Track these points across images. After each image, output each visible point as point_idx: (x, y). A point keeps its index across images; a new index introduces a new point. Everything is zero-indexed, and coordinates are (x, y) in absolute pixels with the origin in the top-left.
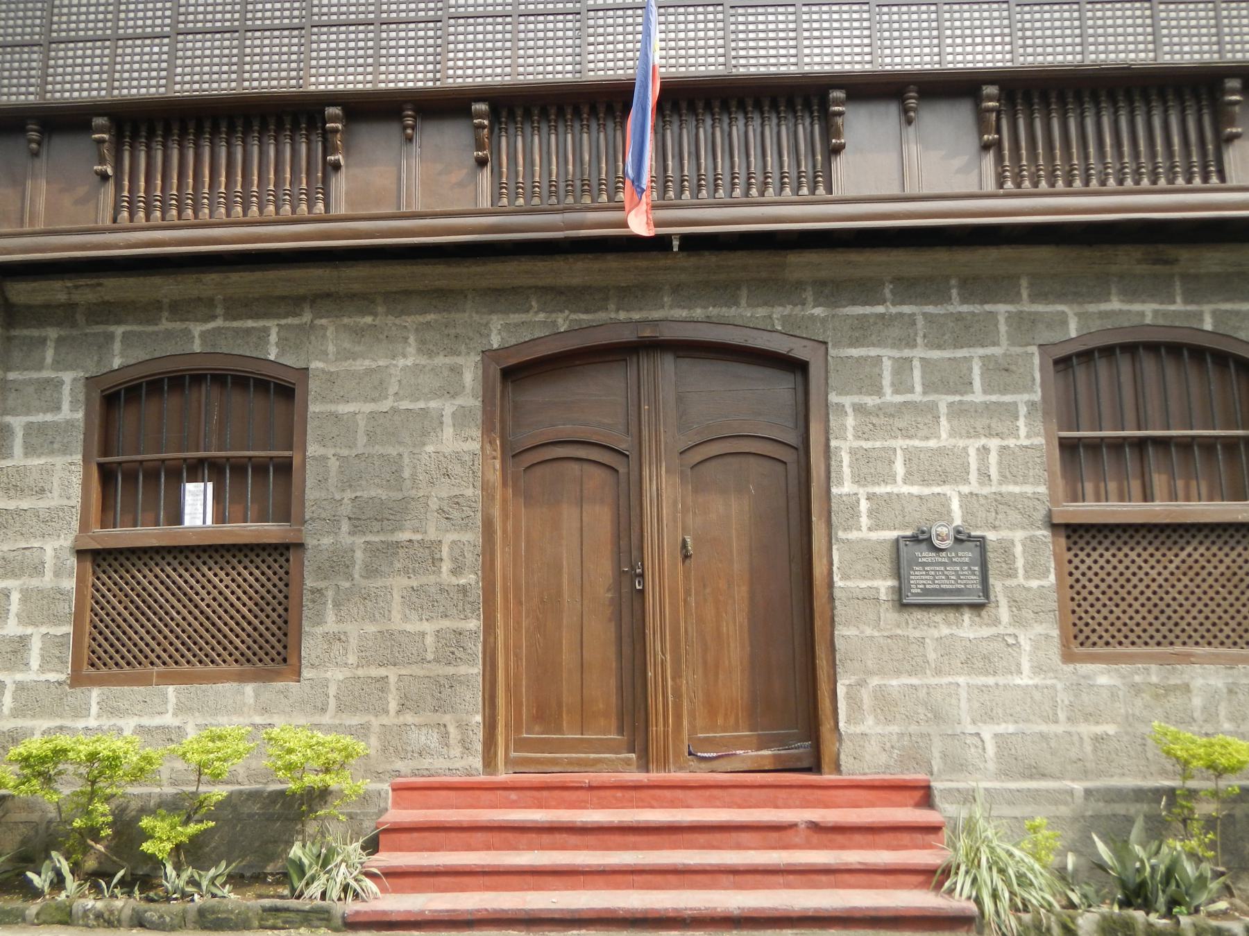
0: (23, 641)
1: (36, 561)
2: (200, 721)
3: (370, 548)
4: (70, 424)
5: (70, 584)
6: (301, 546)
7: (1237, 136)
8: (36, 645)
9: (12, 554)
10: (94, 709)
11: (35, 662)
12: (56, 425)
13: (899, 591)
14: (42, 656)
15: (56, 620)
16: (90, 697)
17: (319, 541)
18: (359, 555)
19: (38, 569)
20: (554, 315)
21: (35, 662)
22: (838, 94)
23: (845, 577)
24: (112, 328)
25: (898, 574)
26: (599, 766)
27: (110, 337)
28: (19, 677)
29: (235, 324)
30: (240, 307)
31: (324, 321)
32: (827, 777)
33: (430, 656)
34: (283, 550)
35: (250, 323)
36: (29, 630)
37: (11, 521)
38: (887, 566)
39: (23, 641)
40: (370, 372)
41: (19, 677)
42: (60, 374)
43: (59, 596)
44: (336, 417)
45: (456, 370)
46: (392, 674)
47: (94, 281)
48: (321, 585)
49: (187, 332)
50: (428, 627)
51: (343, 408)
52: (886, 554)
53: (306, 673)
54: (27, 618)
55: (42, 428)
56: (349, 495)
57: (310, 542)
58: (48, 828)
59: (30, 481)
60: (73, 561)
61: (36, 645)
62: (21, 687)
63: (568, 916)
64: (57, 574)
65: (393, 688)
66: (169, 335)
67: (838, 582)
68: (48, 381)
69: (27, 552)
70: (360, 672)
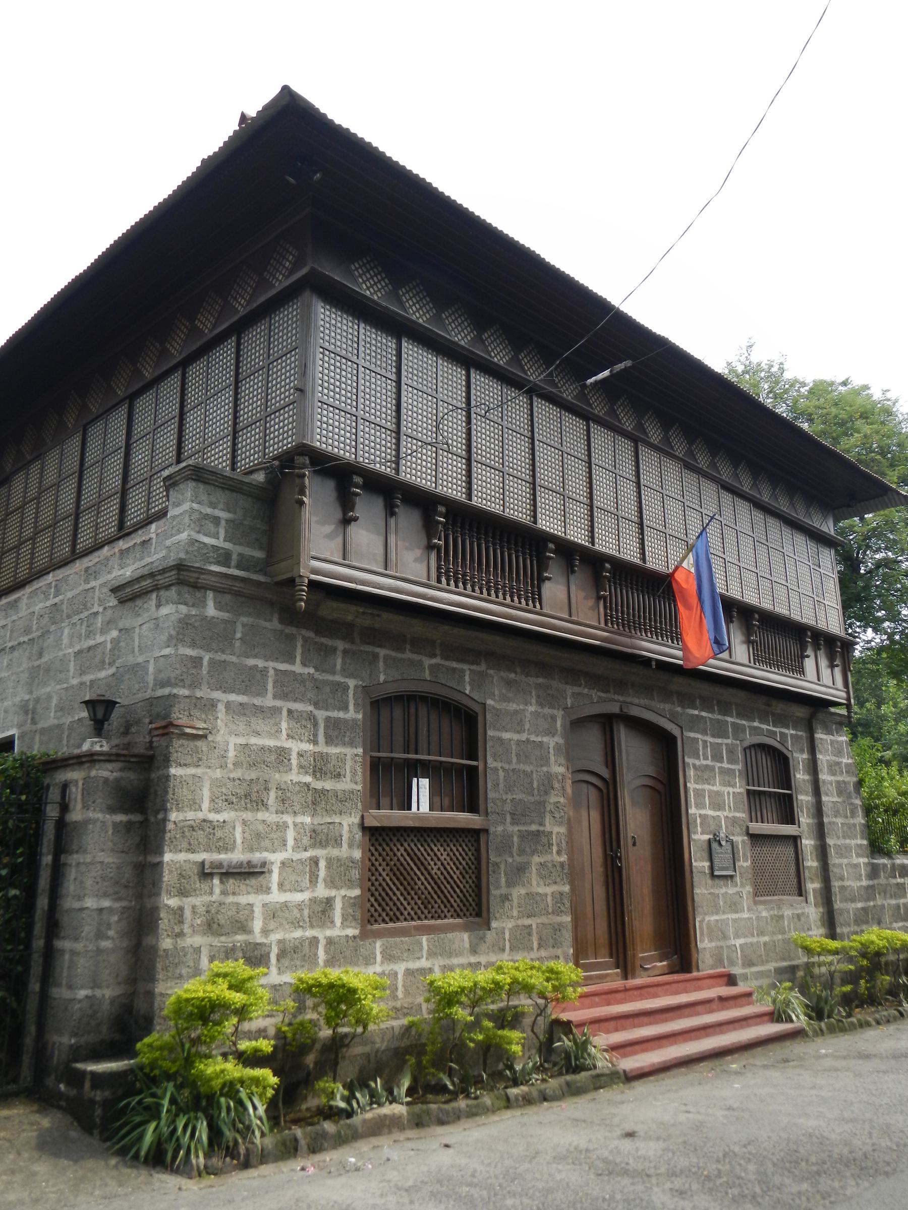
0: (329, 901)
1: (337, 834)
2: (442, 963)
3: (523, 836)
4: (354, 721)
5: (357, 854)
6: (486, 831)
7: (549, 579)
8: (338, 905)
9: (320, 827)
10: (379, 958)
11: (338, 920)
12: (346, 721)
13: (712, 868)
14: (343, 915)
15: (350, 885)
16: (375, 948)
17: (502, 829)
18: (515, 839)
19: (338, 842)
20: (592, 691)
21: (338, 920)
22: (358, 480)
23: (695, 861)
24: (377, 650)
25: (711, 859)
26: (608, 979)
27: (334, 650)
28: (329, 933)
29: (447, 663)
30: (454, 652)
31: (491, 672)
32: (695, 974)
33: (550, 910)
34: (475, 835)
35: (455, 665)
36: (333, 893)
37: (318, 799)
38: (705, 855)
39: (329, 901)
40: (516, 712)
41: (329, 933)
42: (347, 680)
43: (351, 864)
44: (500, 739)
45: (553, 718)
46: (532, 922)
47: (375, 612)
48: (498, 860)
49: (420, 663)
50: (548, 890)
51: (506, 736)
52: (705, 846)
53: (494, 924)
54: (331, 883)
55: (337, 721)
56: (510, 797)
57: (492, 830)
58: (376, 1056)
59: (330, 766)
60: (359, 835)
61: (338, 905)
62: (330, 941)
63: (662, 1066)
64: (350, 846)
65: (534, 932)
66: (412, 663)
67: (694, 864)
68: (339, 684)
69: (331, 827)
70: (520, 922)
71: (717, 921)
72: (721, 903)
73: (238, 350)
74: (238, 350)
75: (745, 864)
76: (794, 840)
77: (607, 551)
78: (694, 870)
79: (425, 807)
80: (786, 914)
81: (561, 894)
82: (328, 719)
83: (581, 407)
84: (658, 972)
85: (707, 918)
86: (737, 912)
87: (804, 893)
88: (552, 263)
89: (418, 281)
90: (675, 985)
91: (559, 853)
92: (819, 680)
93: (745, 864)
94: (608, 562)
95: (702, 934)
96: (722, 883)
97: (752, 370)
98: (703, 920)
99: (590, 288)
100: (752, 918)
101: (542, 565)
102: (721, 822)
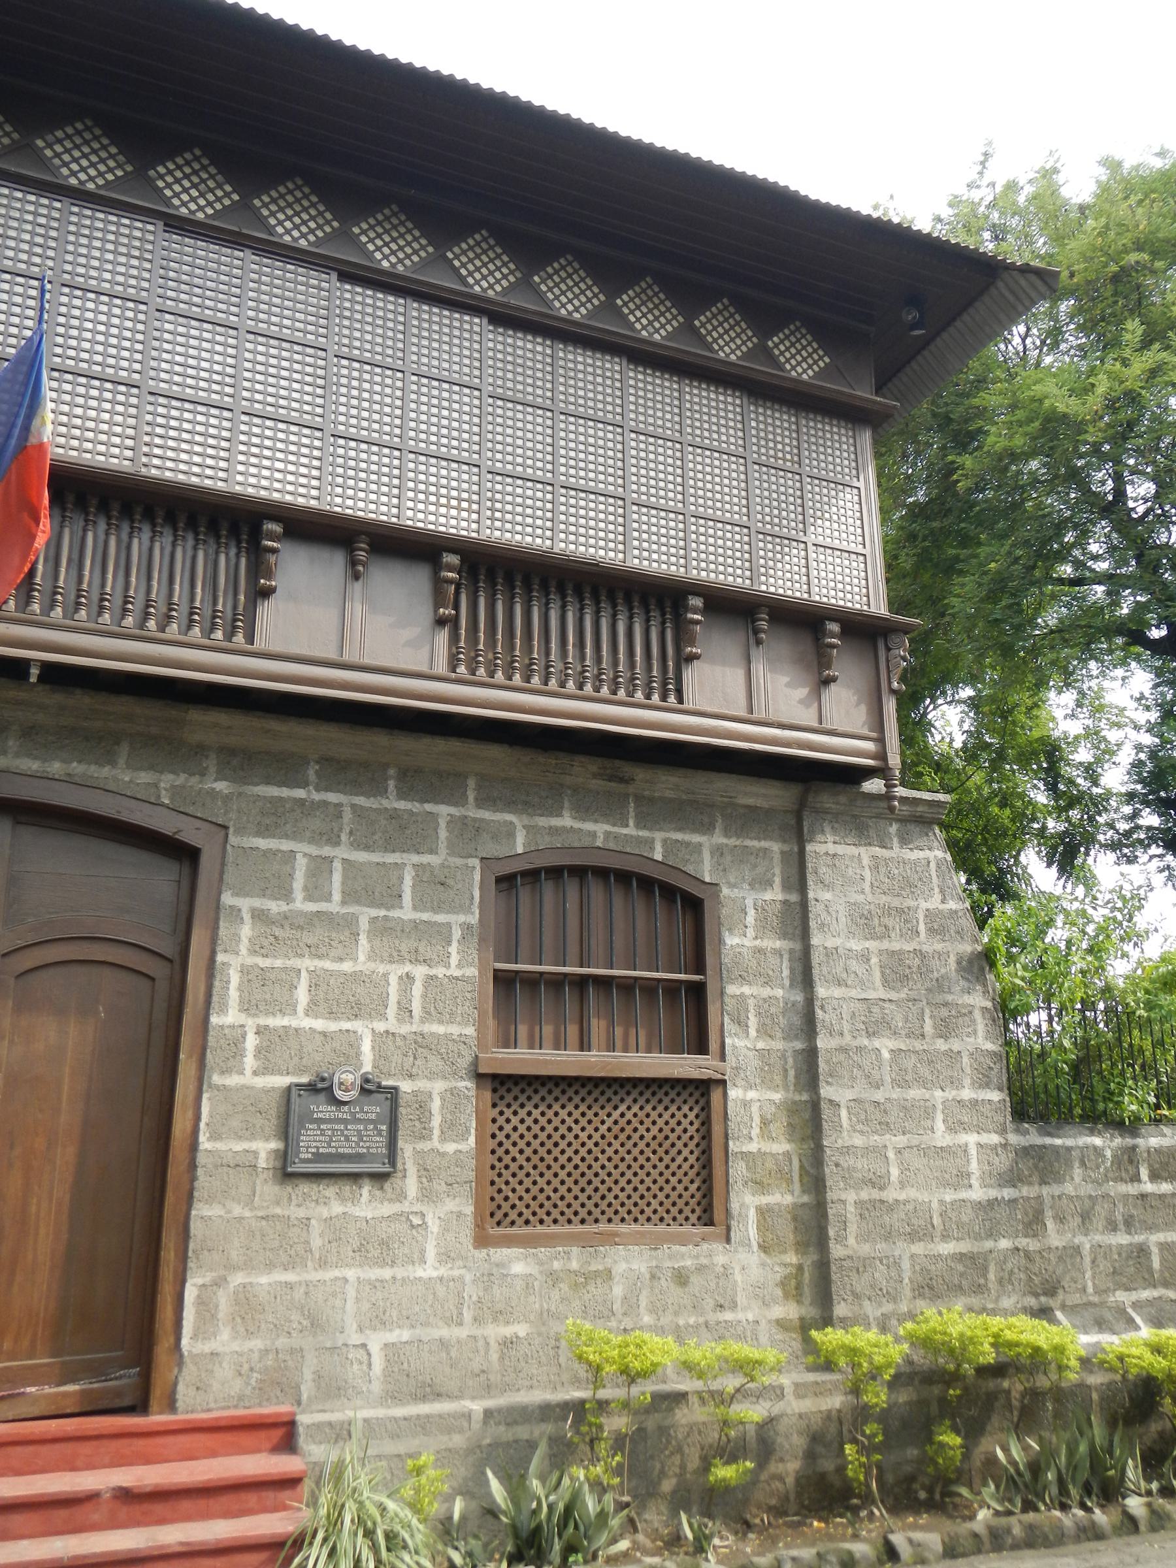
7: (696, 657)
23: (215, 1136)
32: (157, 1418)
76: (702, 1091)
77: (301, 501)
78: (201, 1159)
82: (373, 920)
83: (822, 387)
87: (718, 1215)
88: (670, 147)
89: (725, 301)
92: (751, 712)
94: (454, 551)
97: (971, 220)
99: (717, 162)
101: (683, 633)
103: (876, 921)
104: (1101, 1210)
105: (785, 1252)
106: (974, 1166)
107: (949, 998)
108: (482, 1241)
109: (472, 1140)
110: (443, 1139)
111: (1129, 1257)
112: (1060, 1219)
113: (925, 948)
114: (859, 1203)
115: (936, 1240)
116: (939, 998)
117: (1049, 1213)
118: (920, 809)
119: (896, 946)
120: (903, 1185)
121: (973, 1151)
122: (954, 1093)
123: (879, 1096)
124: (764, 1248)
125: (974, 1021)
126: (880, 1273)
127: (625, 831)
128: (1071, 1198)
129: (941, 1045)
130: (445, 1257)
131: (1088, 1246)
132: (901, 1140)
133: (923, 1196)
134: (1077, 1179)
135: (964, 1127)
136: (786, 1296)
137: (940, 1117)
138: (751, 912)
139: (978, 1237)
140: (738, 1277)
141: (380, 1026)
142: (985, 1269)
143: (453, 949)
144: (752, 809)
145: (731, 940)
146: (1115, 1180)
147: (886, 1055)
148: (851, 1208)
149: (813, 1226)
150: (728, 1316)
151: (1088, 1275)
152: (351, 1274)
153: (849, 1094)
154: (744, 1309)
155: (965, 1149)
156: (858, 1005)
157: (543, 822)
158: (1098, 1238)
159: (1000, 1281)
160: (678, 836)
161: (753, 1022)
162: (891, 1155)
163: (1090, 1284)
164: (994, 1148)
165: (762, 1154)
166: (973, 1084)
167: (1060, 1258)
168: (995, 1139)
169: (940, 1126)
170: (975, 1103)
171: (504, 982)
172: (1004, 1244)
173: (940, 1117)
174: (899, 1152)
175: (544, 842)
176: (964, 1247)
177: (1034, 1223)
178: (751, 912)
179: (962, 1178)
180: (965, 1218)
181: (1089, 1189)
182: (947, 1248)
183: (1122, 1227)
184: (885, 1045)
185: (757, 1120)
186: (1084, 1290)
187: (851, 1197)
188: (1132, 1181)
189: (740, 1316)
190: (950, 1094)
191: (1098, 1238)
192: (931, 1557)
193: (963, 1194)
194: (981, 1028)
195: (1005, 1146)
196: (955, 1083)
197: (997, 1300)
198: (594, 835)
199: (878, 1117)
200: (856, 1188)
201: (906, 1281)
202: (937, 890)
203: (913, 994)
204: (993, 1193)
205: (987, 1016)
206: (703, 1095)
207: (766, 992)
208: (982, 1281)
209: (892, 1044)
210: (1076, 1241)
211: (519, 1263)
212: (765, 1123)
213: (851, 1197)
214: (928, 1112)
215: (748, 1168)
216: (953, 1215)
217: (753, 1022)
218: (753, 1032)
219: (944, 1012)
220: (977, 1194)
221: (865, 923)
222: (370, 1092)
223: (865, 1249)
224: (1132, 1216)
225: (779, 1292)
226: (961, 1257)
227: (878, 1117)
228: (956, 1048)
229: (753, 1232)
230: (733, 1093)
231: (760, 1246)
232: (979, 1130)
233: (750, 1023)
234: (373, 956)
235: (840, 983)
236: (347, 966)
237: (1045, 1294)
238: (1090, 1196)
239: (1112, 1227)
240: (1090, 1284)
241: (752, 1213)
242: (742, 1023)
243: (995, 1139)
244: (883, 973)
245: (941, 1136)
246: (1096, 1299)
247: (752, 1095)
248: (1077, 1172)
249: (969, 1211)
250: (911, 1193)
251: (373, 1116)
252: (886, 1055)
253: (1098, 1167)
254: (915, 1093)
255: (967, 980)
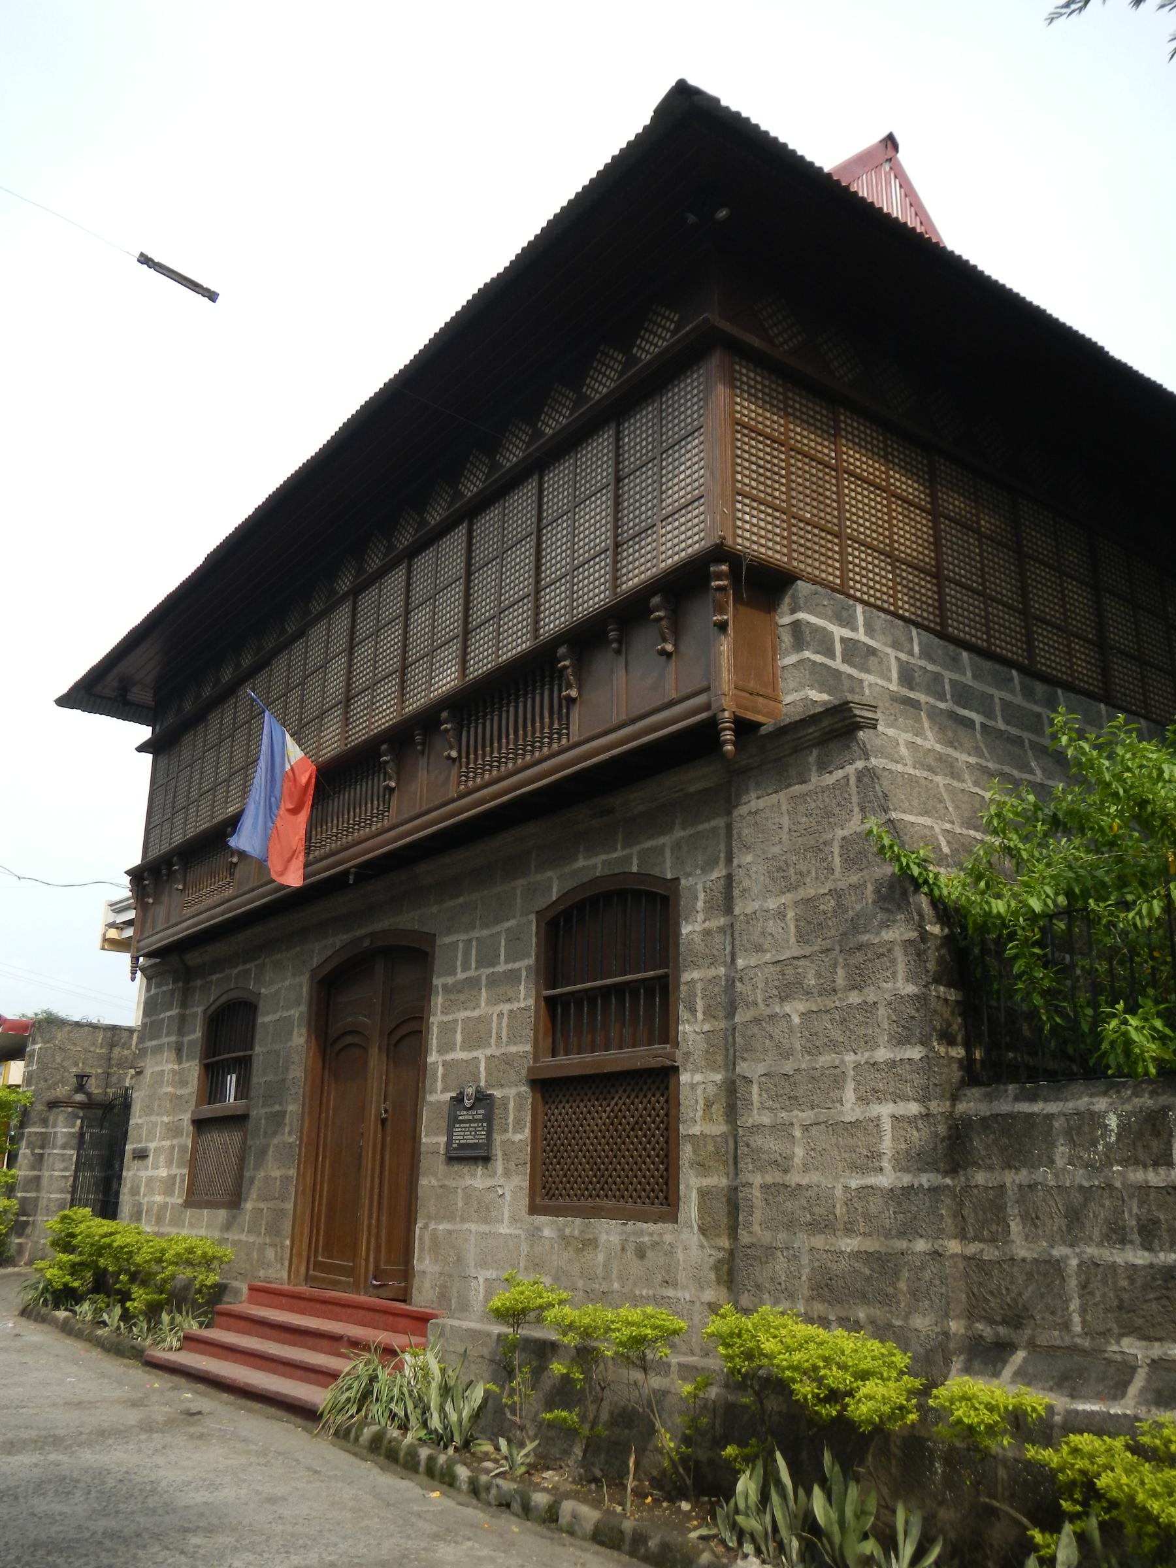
63: (201, 1374)
71: (450, 1232)
72: (460, 1204)
73: (409, 578)
74: (409, 578)
75: (518, 1137)
79: (232, 1100)
80: (603, 1238)
81: (287, 1178)
84: (391, 1295)
85: (432, 1226)
86: (486, 1221)
90: (361, 1312)
91: (290, 1134)
93: (518, 1137)
95: (422, 1250)
96: (465, 1170)
98: (426, 1226)
100: (518, 1237)
102: (478, 1068)
103: (792, 871)
104: (1100, 1211)
105: (719, 1236)
106: (887, 1145)
107: (864, 938)
108: (533, 1209)
109: (527, 1131)
110: (514, 1132)
111: (1146, 1287)
112: (1031, 1219)
113: (841, 885)
114: (765, 1187)
115: (839, 1233)
116: (853, 942)
117: (1013, 1210)
118: (825, 723)
119: (811, 892)
120: (806, 1168)
121: (887, 1125)
122: (867, 1055)
123: (788, 1068)
124: (703, 1230)
125: (893, 961)
126: (780, 1265)
127: (615, 855)
128: (1048, 1190)
129: (854, 998)
130: (514, 1220)
131: (1074, 1262)
132: (808, 1116)
133: (826, 1182)
134: (1060, 1162)
135: (878, 1095)
136: (719, 1281)
137: (850, 1086)
138: (701, 896)
139: (888, 1235)
140: (680, 1256)
141: (488, 1052)
142: (896, 1275)
143: (522, 988)
144: (705, 791)
145: (686, 929)
146: (1125, 1162)
147: (796, 1020)
148: (757, 1193)
149: (731, 1209)
150: (670, 1293)
151: (1075, 1304)
152: (473, 1227)
153: (761, 1069)
154: (684, 1288)
155: (876, 1122)
156: (772, 968)
157: (567, 870)
158: (1091, 1251)
159: (914, 1293)
160: (648, 844)
161: (700, 1005)
162: (798, 1133)
163: (1076, 1319)
164: (912, 1120)
165: (704, 1136)
166: (891, 1037)
167: (1030, 1275)
168: (914, 1108)
169: (849, 1095)
170: (892, 1064)
171: (551, 1002)
172: (921, 1245)
173: (850, 1086)
174: (806, 1129)
175: (571, 884)
176: (871, 1245)
177: (988, 1216)
178: (701, 896)
179: (870, 1162)
180: (873, 1209)
181: (1080, 1177)
182: (849, 1244)
183: (1136, 1237)
184: (795, 1009)
185: (701, 1102)
186: (1066, 1326)
187: (757, 1180)
188: (1156, 1164)
189: (680, 1294)
190: (863, 1056)
191: (1091, 1251)
192: (579, 1534)
193: (872, 1180)
194: (901, 969)
195: (927, 1116)
196: (870, 1043)
197: (906, 1318)
198: (595, 867)
199: (788, 1090)
200: (762, 1170)
201: (804, 1278)
202: (856, 809)
203: (827, 944)
204: (907, 1179)
205: (911, 950)
206: (662, 1082)
207: (712, 972)
208: (890, 1290)
209: (801, 1007)
210: (1056, 1252)
211: (548, 1227)
212: (708, 1105)
213: (757, 1180)
214: (838, 1082)
215: (694, 1151)
216: (859, 1205)
217: (700, 1005)
218: (700, 1016)
219: (859, 957)
220: (886, 1179)
221: (783, 878)
222: (481, 1100)
223: (766, 1237)
224: (1156, 1222)
225: (712, 1276)
226: (866, 1257)
227: (788, 1090)
228: (871, 999)
229: (694, 1214)
230: (684, 1078)
231: (700, 1228)
232: (898, 1097)
233: (698, 1008)
234: (489, 1003)
235: (759, 948)
236: (476, 1013)
237: (1005, 1322)
238: (1081, 1187)
239: (1116, 1235)
240: (1076, 1319)
241: (694, 1194)
242: (693, 1010)
243: (914, 1108)
244: (797, 927)
245: (850, 1108)
246: (1087, 1343)
247: (698, 1078)
248: (1061, 1151)
249: (880, 1201)
250: (814, 1177)
251: (481, 1117)
252: (796, 1020)
253: (1094, 1143)
254: (825, 1060)
255: (887, 910)
